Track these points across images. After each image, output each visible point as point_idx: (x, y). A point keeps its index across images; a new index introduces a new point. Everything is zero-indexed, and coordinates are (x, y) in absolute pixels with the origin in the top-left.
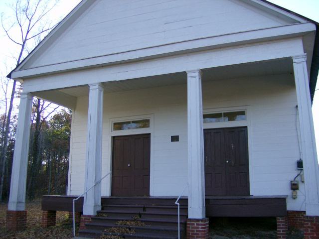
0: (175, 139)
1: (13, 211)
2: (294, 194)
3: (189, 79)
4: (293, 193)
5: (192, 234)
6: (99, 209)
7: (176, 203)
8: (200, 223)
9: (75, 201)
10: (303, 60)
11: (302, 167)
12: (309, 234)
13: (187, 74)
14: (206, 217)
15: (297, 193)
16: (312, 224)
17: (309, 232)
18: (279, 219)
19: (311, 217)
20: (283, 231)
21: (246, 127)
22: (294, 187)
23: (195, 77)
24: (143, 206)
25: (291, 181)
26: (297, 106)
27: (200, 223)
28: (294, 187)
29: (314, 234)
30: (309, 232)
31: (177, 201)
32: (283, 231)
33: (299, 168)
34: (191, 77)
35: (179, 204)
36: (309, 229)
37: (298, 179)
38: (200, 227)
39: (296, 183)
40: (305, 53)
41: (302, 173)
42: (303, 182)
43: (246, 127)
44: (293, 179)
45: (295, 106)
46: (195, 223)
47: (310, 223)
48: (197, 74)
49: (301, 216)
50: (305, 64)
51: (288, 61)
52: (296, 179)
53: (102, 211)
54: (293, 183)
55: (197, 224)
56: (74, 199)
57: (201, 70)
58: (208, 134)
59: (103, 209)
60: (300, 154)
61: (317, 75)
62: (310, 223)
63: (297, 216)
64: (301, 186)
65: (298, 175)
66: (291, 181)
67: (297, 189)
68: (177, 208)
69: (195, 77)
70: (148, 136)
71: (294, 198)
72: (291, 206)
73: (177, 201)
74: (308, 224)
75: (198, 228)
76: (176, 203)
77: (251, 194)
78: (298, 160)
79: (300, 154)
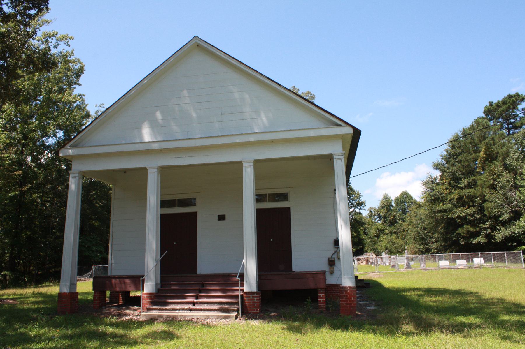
0: (222, 218)
1: (66, 293)
2: (331, 270)
4: (330, 269)
5: (254, 299)
6: (159, 286)
8: (255, 295)
10: (342, 157)
11: (339, 245)
12: (344, 301)
15: (333, 269)
17: (344, 299)
18: (320, 291)
21: (289, 208)
22: (332, 263)
23: (250, 166)
25: (329, 258)
26: (335, 190)
27: (255, 295)
28: (331, 272)
31: (238, 277)
35: (239, 279)
36: (344, 297)
37: (335, 256)
38: (255, 298)
40: (343, 151)
41: (338, 251)
42: (339, 259)
43: (289, 208)
44: (330, 256)
45: (334, 189)
46: (251, 296)
49: (337, 289)
50: (343, 160)
51: (330, 158)
52: (333, 256)
53: (162, 288)
54: (330, 259)
55: (253, 297)
57: (255, 160)
58: (260, 213)
59: (162, 286)
61: (354, 160)
63: (333, 289)
65: (335, 252)
66: (329, 258)
67: (334, 265)
68: (239, 284)
70: (195, 214)
71: (332, 273)
72: (331, 280)
73: (238, 277)
74: (343, 293)
75: (254, 299)
77: (293, 270)
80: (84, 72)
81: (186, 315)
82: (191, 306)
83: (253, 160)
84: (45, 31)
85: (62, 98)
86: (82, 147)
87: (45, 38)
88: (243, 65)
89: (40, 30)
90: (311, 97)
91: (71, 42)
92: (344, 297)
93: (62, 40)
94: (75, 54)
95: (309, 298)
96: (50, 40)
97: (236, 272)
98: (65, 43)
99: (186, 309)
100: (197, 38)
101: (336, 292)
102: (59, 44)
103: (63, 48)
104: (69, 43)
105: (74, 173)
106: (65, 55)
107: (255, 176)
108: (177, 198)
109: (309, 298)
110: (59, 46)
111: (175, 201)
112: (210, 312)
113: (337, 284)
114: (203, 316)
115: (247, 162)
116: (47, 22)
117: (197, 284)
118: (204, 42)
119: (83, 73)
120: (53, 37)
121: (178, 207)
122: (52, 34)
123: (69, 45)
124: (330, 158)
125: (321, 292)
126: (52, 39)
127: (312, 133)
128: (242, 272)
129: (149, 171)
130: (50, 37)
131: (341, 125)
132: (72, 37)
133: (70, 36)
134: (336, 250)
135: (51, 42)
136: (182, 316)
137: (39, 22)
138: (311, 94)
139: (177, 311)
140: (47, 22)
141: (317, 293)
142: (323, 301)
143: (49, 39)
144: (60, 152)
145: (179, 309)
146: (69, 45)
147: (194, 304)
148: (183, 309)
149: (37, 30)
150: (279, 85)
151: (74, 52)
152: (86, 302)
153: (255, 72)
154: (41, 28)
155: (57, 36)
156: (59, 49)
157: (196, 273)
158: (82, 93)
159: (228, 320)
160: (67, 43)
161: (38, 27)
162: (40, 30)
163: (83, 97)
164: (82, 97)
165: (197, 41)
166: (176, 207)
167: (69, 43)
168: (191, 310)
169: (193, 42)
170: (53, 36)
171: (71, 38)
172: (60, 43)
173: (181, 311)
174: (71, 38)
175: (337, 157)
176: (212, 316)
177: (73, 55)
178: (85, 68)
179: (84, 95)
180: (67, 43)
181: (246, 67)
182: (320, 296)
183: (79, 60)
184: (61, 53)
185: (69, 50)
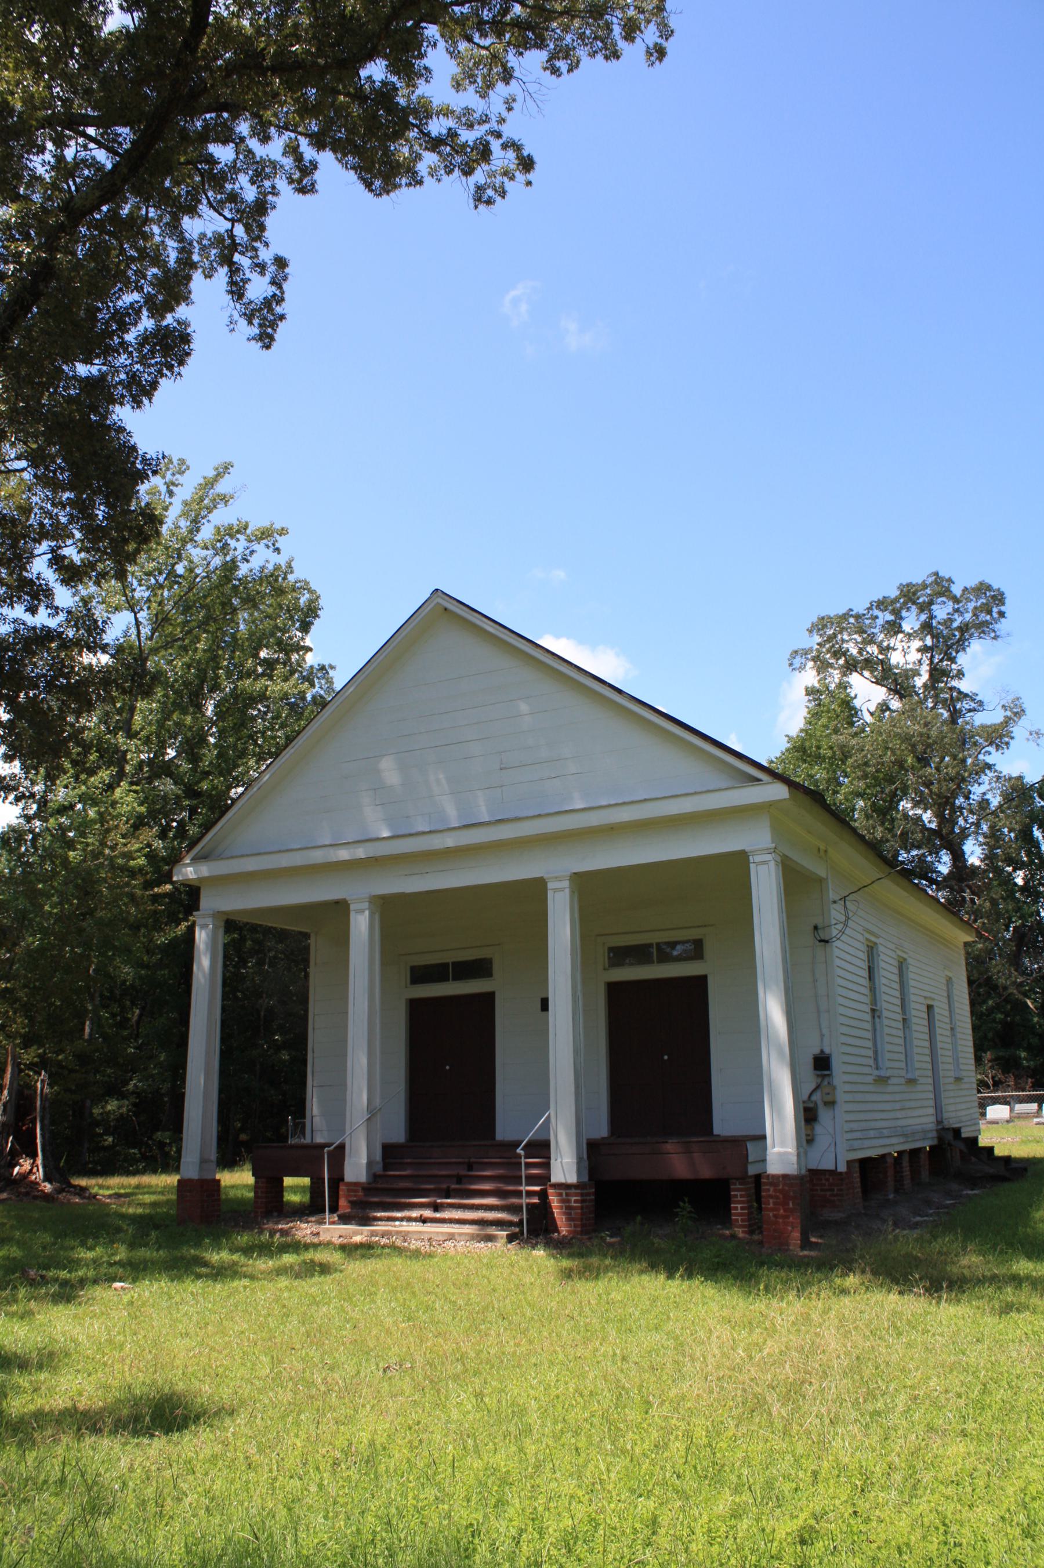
3: (550, 894)
6: (378, 1169)
7: (519, 1151)
9: (329, 1153)
13: (546, 883)
14: (590, 1180)
16: (775, 1191)
19: (773, 1176)
20: (742, 1208)
24: (466, 1160)
27: (573, 1191)
29: (778, 1210)
30: (771, 1205)
32: (742, 1208)
33: (819, 1073)
34: (555, 890)
36: (771, 1201)
38: (573, 1199)
39: (811, 1105)
47: (772, 1189)
48: (566, 884)
51: (739, 861)
52: (814, 1098)
55: (567, 1195)
56: (326, 1150)
57: (575, 873)
59: (386, 1167)
60: (822, 1040)
62: (772, 1189)
64: (824, 1114)
65: (818, 1087)
69: (562, 890)
70: (489, 998)
76: (519, 1151)
77: (716, 1131)
78: (817, 1051)
79: (822, 1040)
80: (319, 612)
81: (408, 1232)
82: (428, 1213)
83: (569, 874)
84: (218, 523)
85: (266, 690)
86: (220, 858)
87: (220, 541)
88: (539, 650)
89: (209, 521)
90: (993, 597)
91: (282, 542)
92: (771, 1201)
93: (259, 539)
94: (295, 568)
95: (686, 1199)
96: (232, 543)
97: (520, 1139)
98: (268, 547)
99: (415, 1220)
100: (439, 593)
101: (822, 1190)
102: (252, 552)
103: (262, 558)
104: (277, 545)
105: (204, 916)
106: (271, 576)
107: (581, 909)
108: (450, 960)
109: (686, 1199)
110: (255, 555)
111: (445, 966)
112: (462, 1226)
113: (820, 1168)
114: (442, 1233)
115: (557, 879)
116: (225, 499)
117: (460, 1163)
118: (455, 602)
119: (318, 616)
120: (238, 536)
121: (454, 979)
122: (236, 528)
123: (277, 550)
124: (739, 861)
125: (738, 1186)
126: (238, 540)
127: (687, 806)
128: (541, 1137)
129: (352, 907)
130: (232, 537)
131: (759, 780)
132: (283, 529)
133: (278, 526)
134: (819, 1080)
135: (235, 549)
136: (401, 1232)
137: (206, 502)
138: (989, 588)
139: (397, 1223)
140: (225, 499)
141: (729, 1190)
142: (736, 1208)
143: (229, 541)
144: (175, 871)
145: (401, 1219)
146: (277, 550)
147: (436, 1208)
148: (410, 1219)
149: (203, 521)
150: (619, 691)
151: (293, 564)
152: (241, 1202)
153: (565, 664)
154: (211, 517)
155: (249, 531)
156: (256, 562)
157: (494, 1138)
158: (326, 663)
159: (490, 1244)
160: (274, 545)
161: (203, 513)
162: (209, 521)
163: (331, 673)
164: (327, 673)
165: (440, 600)
166: (448, 980)
167: (277, 545)
168: (424, 1220)
169: (432, 605)
170: (238, 532)
171: (283, 532)
172: (255, 547)
173: (404, 1223)
174: (283, 532)
175: (758, 858)
176: (461, 1234)
177: (292, 572)
178: (322, 602)
179: (332, 667)
180: (274, 545)
181: (546, 654)
182: (736, 1196)
183: (307, 583)
184: (262, 568)
185: (282, 560)
